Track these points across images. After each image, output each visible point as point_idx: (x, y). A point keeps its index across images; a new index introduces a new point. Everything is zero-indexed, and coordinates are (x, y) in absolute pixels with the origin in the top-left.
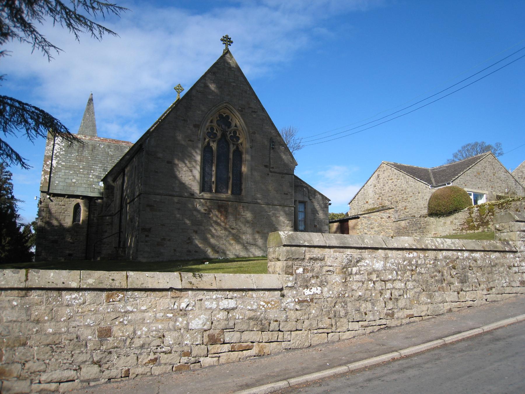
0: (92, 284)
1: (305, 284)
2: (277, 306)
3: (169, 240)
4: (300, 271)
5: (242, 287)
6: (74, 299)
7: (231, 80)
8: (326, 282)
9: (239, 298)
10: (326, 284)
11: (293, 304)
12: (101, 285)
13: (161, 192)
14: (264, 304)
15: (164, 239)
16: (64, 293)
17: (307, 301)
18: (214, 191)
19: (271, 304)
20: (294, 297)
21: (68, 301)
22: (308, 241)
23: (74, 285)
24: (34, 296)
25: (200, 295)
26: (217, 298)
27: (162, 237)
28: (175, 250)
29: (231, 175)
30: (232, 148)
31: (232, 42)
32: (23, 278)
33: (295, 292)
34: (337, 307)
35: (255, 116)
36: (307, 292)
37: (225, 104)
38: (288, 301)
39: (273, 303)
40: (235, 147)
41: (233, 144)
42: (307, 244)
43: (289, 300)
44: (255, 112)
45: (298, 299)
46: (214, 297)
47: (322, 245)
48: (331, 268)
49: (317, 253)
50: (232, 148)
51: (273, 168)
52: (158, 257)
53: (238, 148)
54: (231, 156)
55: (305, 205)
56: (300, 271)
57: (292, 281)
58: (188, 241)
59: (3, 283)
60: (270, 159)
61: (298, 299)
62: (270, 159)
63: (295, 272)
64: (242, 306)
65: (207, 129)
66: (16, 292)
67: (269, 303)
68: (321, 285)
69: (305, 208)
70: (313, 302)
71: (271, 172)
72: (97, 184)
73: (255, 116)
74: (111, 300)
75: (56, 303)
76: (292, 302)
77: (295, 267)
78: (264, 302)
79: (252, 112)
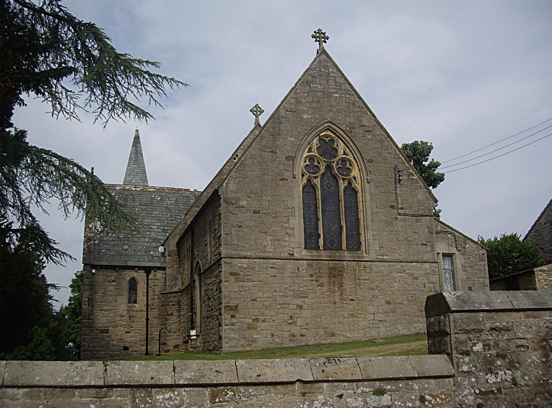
0: (190, 379)
1: (489, 366)
2: (449, 401)
3: (264, 321)
4: (479, 347)
5: (388, 376)
6: (167, 399)
7: (332, 91)
8: (518, 363)
9: (394, 391)
10: (518, 365)
11: (472, 398)
12: (202, 379)
13: (249, 254)
14: (431, 398)
15: (257, 320)
16: (154, 390)
17: (492, 392)
18: (321, 248)
19: (441, 399)
20: (473, 387)
21: (161, 403)
22: (487, 304)
23: (168, 380)
24: (115, 397)
25: (342, 389)
26: (363, 392)
27: (254, 318)
28: (273, 335)
29: (343, 224)
30: (342, 185)
31: (328, 38)
32: (101, 374)
33: (473, 380)
34: (538, 399)
35: (369, 137)
36: (492, 379)
37: (326, 125)
38: (465, 393)
39: (443, 397)
40: (346, 184)
41: (343, 179)
42: (486, 308)
43: (466, 392)
44: (369, 131)
45: (480, 390)
46: (359, 391)
47: (507, 308)
48: (523, 342)
49: (503, 320)
50: (342, 185)
51: (402, 208)
52: (250, 345)
53: (350, 183)
54: (342, 193)
55: (452, 259)
56: (479, 347)
57: (468, 364)
58: (290, 321)
59: (77, 379)
60: (396, 196)
61: (480, 390)
62: (396, 196)
63: (472, 349)
64: (399, 403)
65: (305, 161)
66: (93, 391)
67: (437, 396)
68: (511, 366)
69: (452, 263)
70: (501, 393)
71: (399, 214)
72: (157, 250)
73: (369, 137)
74: (217, 400)
75: (145, 405)
76: (471, 395)
77: (470, 344)
78: (431, 396)
79: (366, 131)
